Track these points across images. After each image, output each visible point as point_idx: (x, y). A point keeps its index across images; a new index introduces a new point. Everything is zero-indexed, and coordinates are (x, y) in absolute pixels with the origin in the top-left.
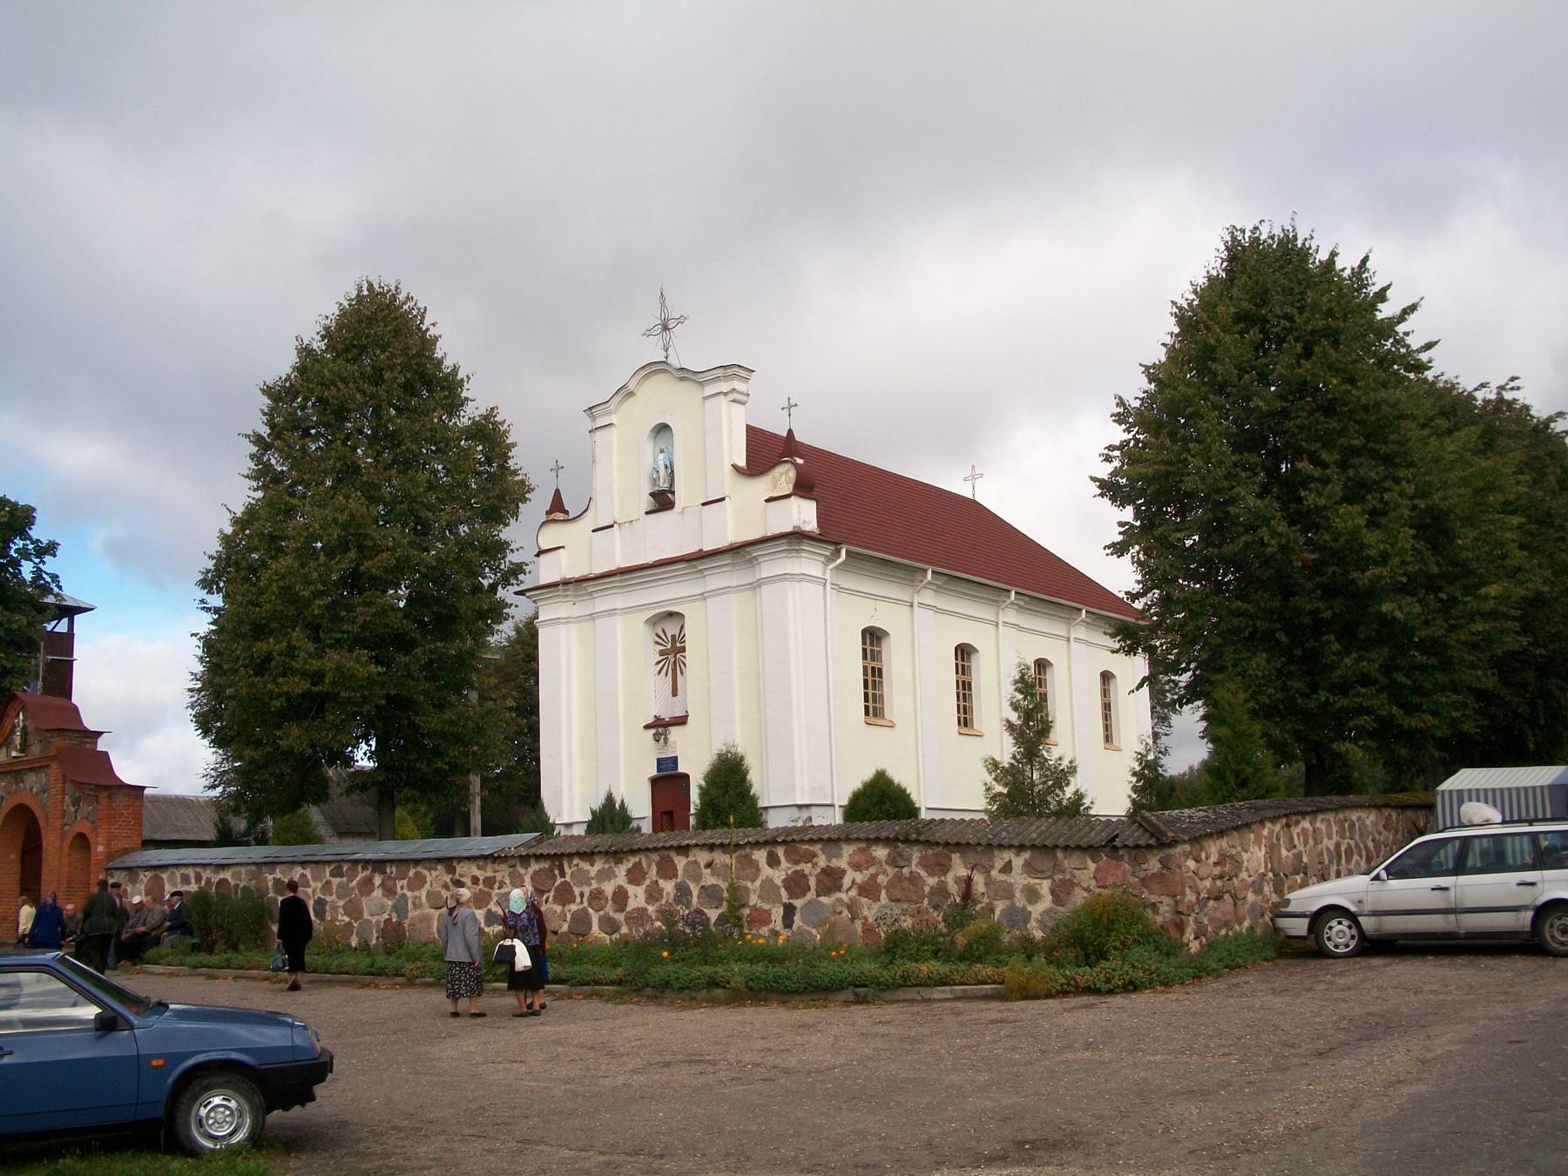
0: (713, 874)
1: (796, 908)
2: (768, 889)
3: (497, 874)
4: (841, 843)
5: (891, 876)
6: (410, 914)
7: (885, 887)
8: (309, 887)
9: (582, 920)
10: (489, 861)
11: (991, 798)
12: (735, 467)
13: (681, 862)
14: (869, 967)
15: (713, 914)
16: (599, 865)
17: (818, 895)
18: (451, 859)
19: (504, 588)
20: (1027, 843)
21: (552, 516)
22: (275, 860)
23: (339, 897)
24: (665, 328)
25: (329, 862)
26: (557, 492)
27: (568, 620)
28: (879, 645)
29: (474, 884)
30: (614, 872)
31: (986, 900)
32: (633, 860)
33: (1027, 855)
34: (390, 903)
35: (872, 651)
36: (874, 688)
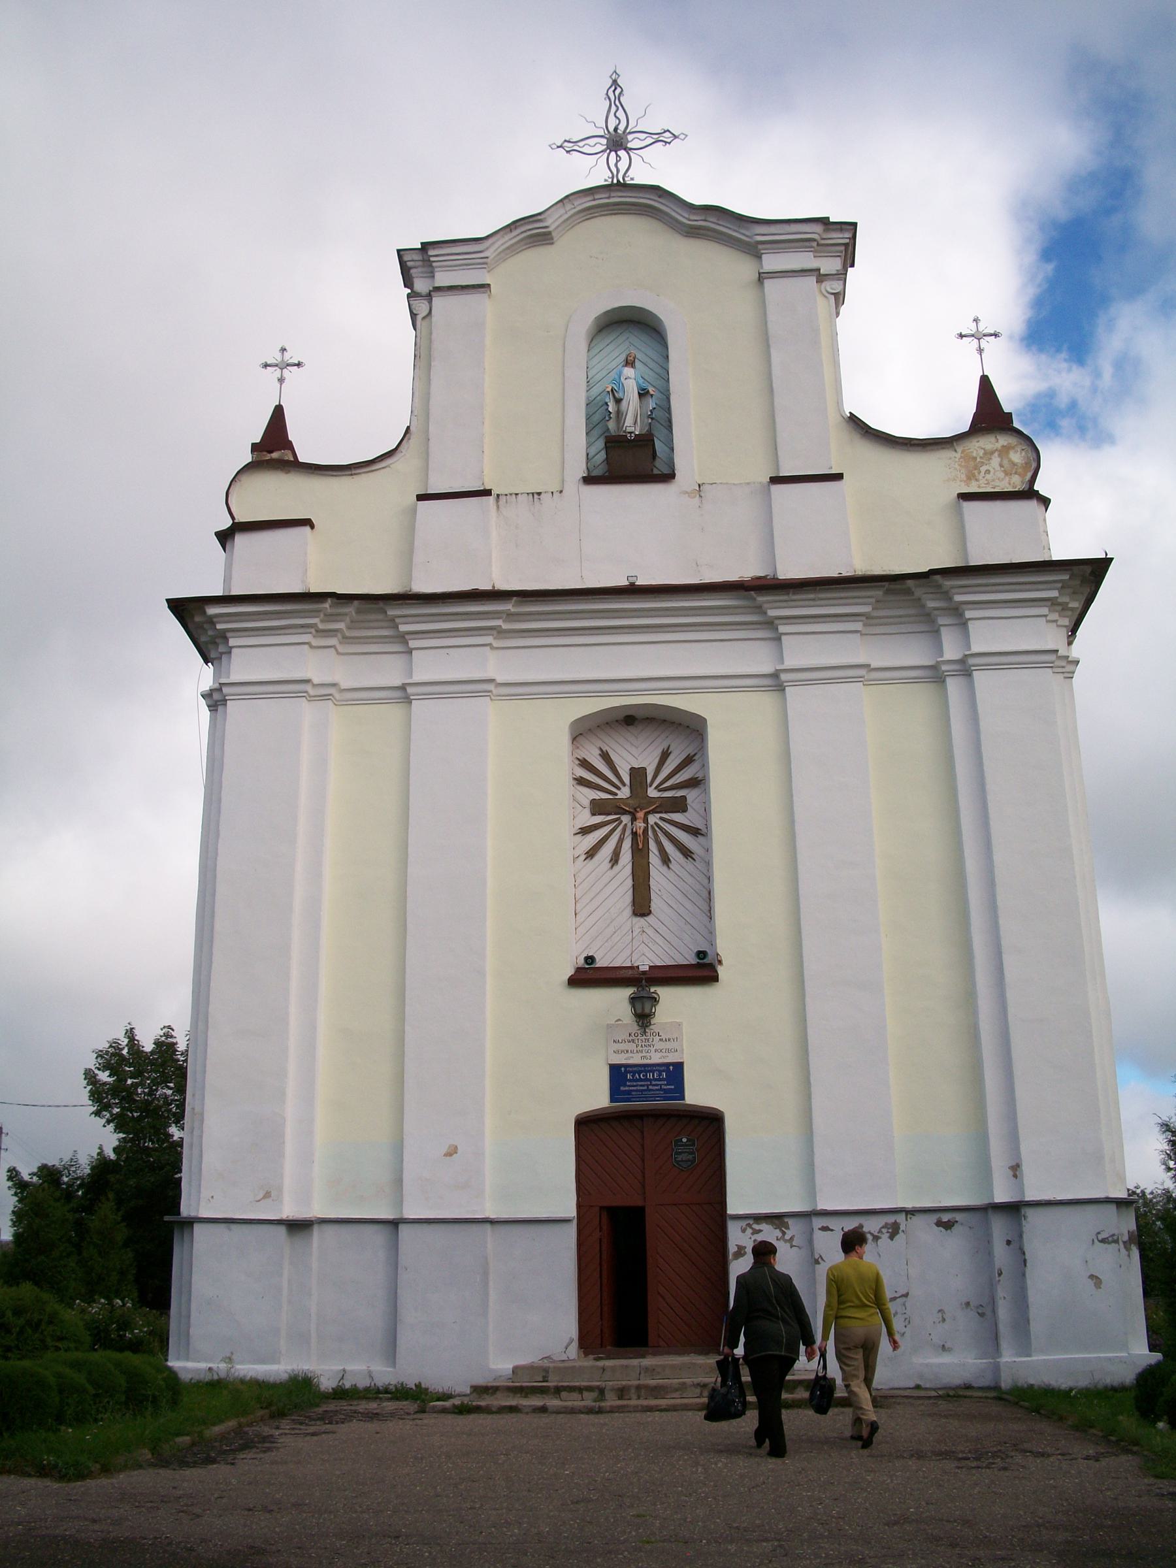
26: (278, 413)
27: (327, 693)
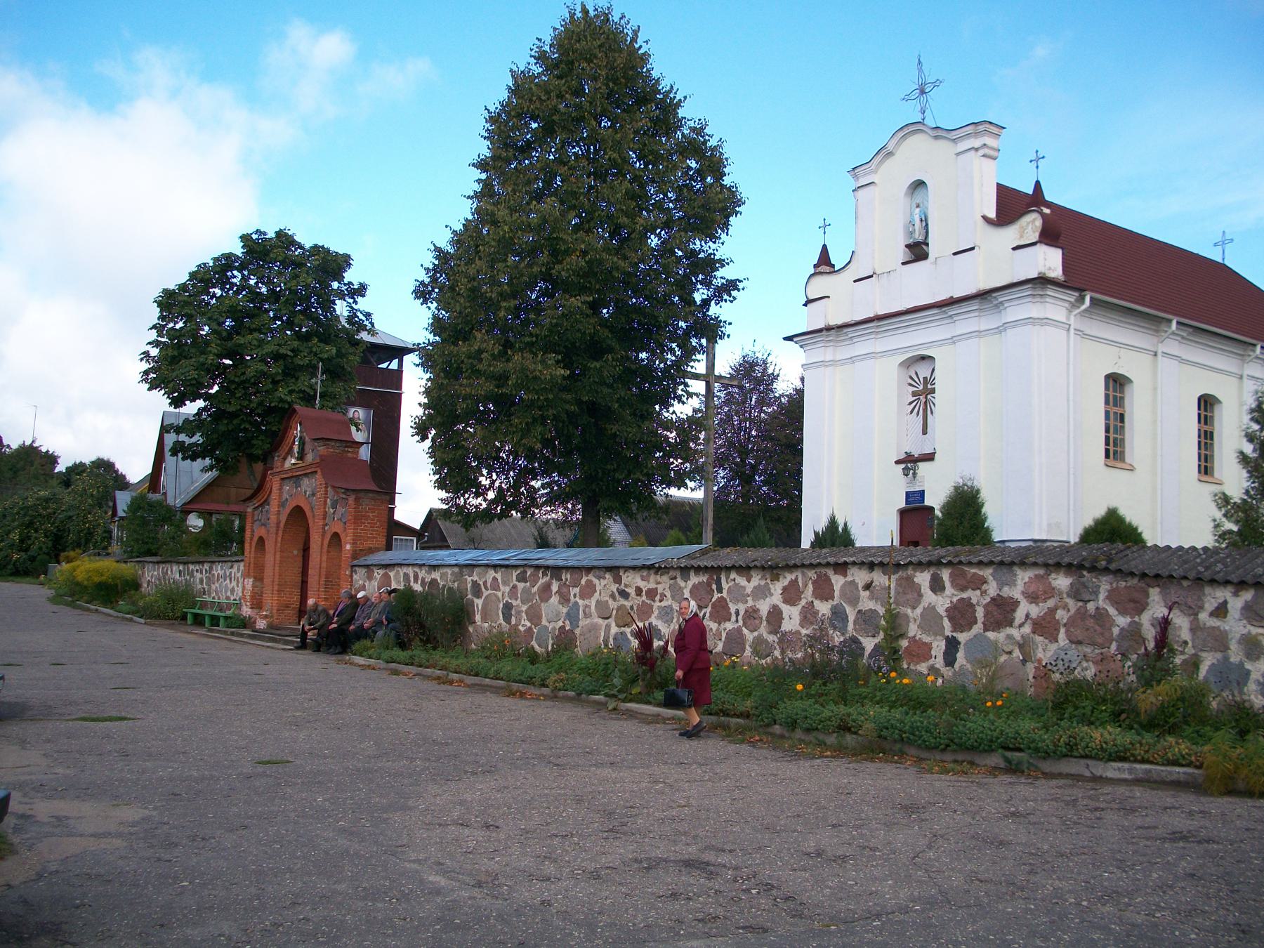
0: (871, 598)
1: (959, 643)
2: (930, 620)
3: (659, 586)
4: (1015, 568)
5: (1072, 611)
6: (581, 623)
7: (1065, 625)
8: (500, 590)
9: (735, 640)
10: (652, 572)
11: (1220, 536)
12: (984, 218)
13: (838, 581)
14: (1027, 725)
15: (869, 644)
16: (756, 580)
17: (986, 630)
18: (618, 568)
19: (717, 304)
20: (1249, 579)
21: (820, 269)
22: (474, 562)
23: (523, 603)
24: (923, 92)
25: (516, 567)
26: (825, 248)
28: (1122, 391)
29: (637, 595)
30: (769, 589)
31: (1190, 650)
32: (788, 578)
33: (1248, 595)
34: (565, 610)
35: (1115, 397)
36: (1115, 432)
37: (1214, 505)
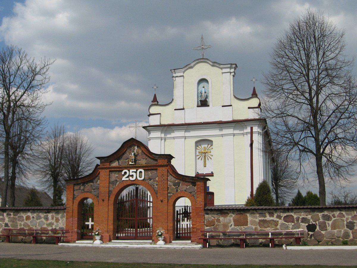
37: (213, 146)
